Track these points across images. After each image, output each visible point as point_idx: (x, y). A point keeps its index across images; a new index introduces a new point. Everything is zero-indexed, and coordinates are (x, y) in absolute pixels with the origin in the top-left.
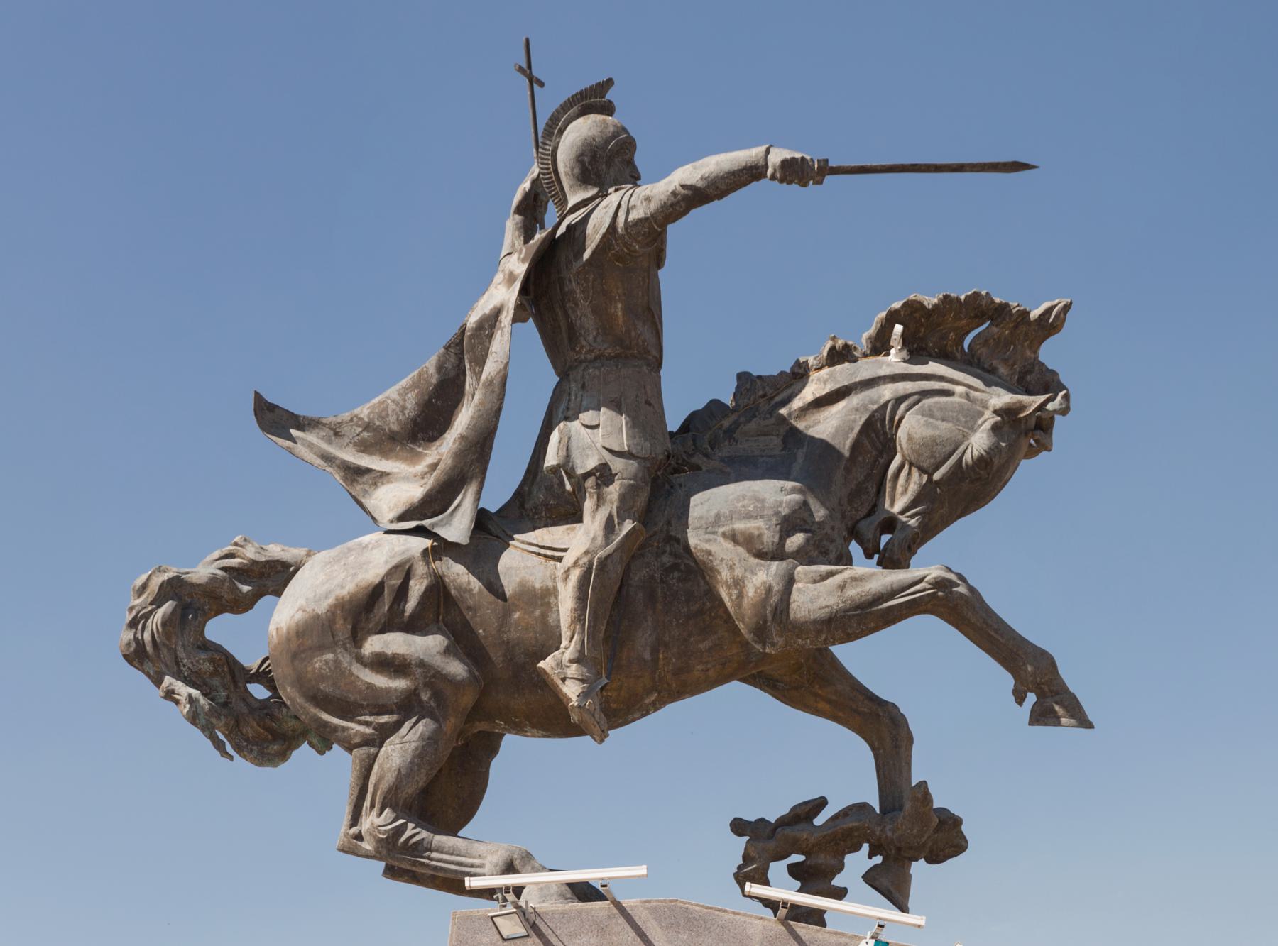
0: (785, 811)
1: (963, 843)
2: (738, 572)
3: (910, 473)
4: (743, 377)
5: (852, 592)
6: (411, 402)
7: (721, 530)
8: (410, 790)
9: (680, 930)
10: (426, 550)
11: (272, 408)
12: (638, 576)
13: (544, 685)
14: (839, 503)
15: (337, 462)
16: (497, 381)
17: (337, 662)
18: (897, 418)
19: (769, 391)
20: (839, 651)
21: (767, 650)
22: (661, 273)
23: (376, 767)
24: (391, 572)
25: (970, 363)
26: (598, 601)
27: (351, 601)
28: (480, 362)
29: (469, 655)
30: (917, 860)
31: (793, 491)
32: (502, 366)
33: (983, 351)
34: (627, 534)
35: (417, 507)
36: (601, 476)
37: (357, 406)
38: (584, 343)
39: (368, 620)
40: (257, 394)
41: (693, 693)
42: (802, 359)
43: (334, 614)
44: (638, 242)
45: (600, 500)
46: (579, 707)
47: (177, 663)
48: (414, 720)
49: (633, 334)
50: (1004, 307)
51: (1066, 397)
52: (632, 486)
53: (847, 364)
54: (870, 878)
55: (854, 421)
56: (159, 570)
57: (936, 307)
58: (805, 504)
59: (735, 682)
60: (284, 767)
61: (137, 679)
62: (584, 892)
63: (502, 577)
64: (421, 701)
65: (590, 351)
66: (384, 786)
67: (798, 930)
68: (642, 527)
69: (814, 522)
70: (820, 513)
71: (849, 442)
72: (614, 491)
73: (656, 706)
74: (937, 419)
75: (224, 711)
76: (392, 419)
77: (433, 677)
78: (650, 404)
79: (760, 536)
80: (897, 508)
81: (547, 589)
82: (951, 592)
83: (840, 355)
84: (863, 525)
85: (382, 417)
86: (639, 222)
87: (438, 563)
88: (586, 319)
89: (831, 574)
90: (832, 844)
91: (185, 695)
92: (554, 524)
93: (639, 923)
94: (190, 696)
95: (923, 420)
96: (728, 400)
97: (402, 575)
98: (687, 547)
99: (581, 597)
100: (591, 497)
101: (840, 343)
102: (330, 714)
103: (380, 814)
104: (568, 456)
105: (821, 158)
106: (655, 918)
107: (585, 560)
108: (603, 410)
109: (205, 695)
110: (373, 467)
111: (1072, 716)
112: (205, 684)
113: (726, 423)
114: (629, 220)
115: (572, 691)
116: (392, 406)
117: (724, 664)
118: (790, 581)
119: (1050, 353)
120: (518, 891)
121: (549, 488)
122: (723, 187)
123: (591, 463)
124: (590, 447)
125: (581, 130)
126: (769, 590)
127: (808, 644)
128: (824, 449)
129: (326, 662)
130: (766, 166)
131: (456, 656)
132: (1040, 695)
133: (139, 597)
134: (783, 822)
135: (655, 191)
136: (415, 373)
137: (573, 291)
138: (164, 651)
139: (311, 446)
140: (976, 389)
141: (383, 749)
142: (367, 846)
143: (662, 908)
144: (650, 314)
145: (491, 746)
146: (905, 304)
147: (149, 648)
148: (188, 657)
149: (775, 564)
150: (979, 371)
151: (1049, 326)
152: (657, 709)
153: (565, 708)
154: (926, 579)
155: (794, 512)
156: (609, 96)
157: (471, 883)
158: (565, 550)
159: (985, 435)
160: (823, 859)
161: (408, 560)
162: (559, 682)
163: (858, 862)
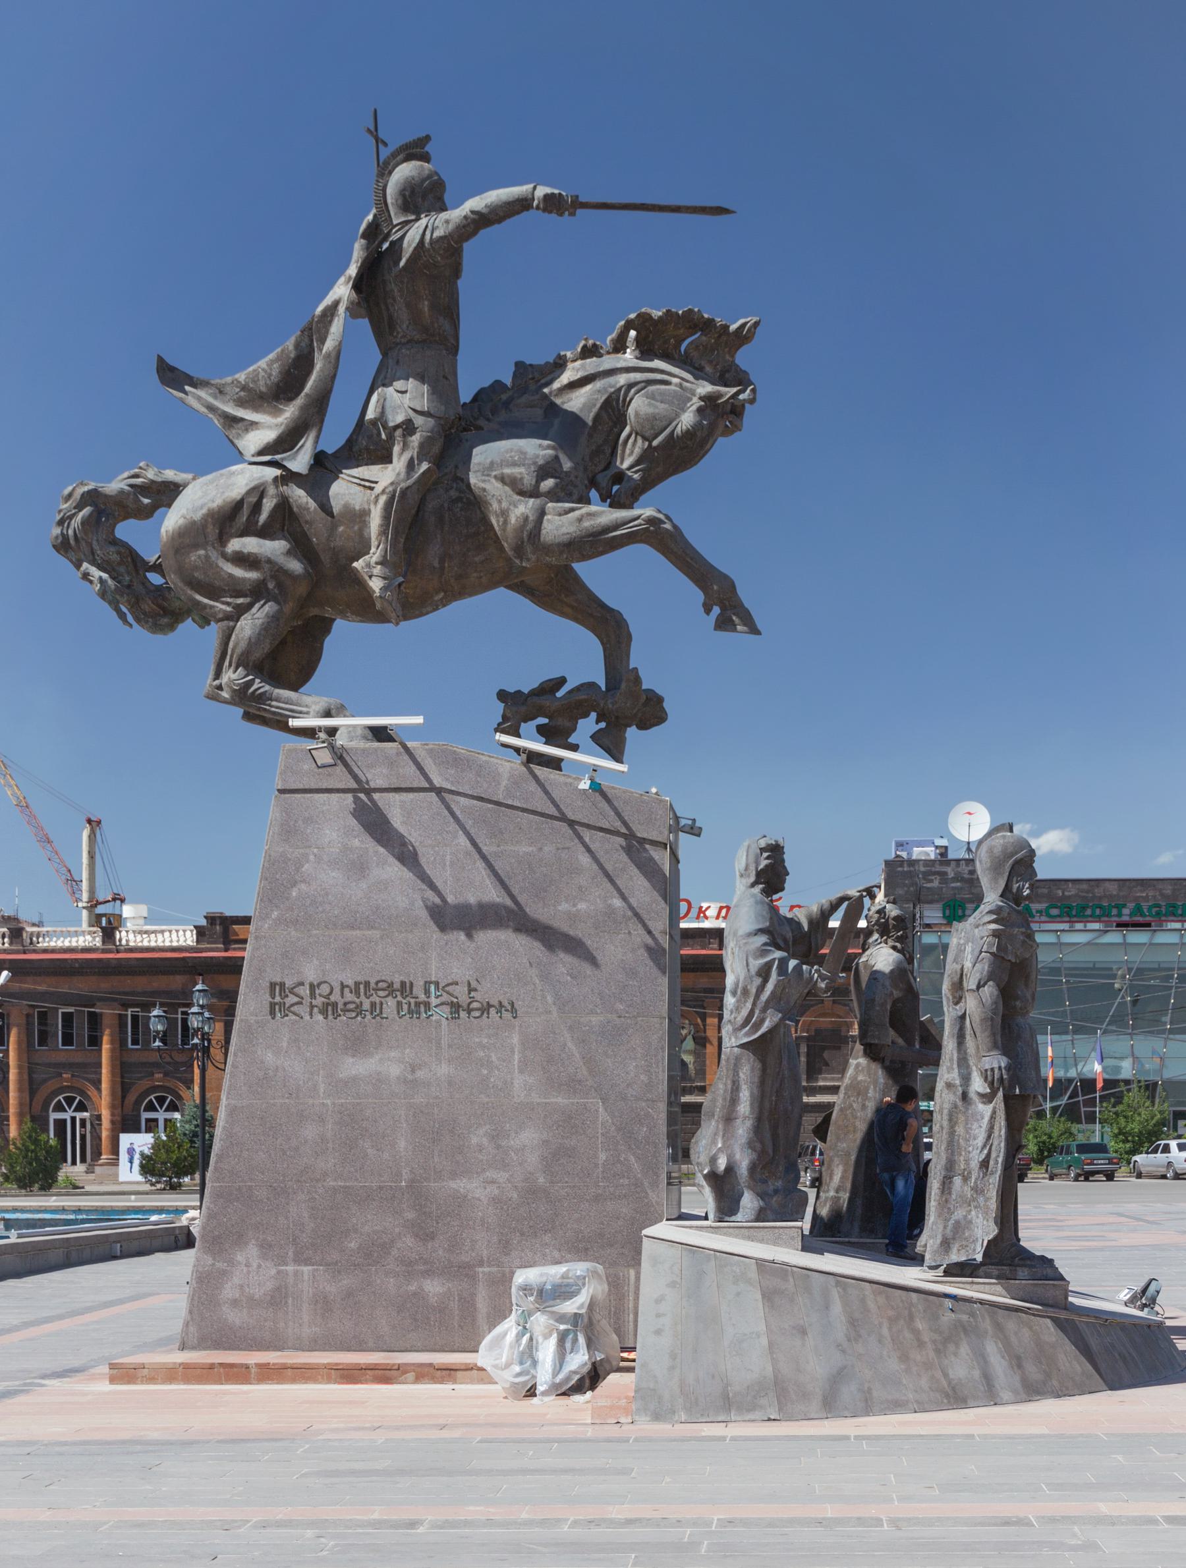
0: (536, 685)
2: (504, 505)
3: (635, 440)
4: (519, 365)
5: (587, 524)
6: (276, 370)
7: (494, 473)
8: (257, 654)
10: (276, 477)
11: (172, 369)
12: (431, 505)
13: (357, 582)
14: (583, 459)
15: (219, 412)
16: (333, 355)
17: (207, 557)
18: (628, 399)
19: (537, 375)
20: (581, 568)
21: (524, 564)
22: (459, 282)
23: (234, 636)
24: (250, 492)
25: (685, 363)
26: (399, 520)
27: (219, 512)
28: (323, 341)
29: (305, 557)
30: (630, 726)
31: (549, 447)
32: (337, 343)
33: (695, 354)
34: (424, 473)
36: (407, 428)
37: (238, 372)
38: (400, 330)
39: (231, 526)
40: (160, 360)
41: (471, 595)
42: (562, 353)
43: (206, 520)
44: (440, 255)
45: (405, 446)
46: (380, 597)
47: (93, 553)
48: (262, 602)
49: (436, 325)
50: (710, 322)
51: (753, 391)
52: (429, 437)
53: (594, 359)
54: (595, 737)
55: (597, 399)
56: (82, 484)
57: (660, 317)
58: (556, 458)
60: (172, 636)
61: (63, 563)
62: (380, 734)
63: (331, 500)
64: (267, 589)
65: (404, 337)
66: (239, 651)
67: (536, 771)
68: (435, 468)
69: (562, 471)
70: (567, 465)
71: (592, 415)
72: (415, 440)
73: (445, 603)
74: (657, 401)
75: (127, 591)
76: (262, 383)
77: (278, 572)
78: (447, 378)
79: (522, 479)
80: (625, 465)
81: (364, 510)
82: (660, 528)
83: (590, 352)
84: (600, 478)
85: (255, 381)
86: (441, 238)
87: (285, 487)
88: (401, 313)
89: (572, 510)
91: (97, 576)
92: (373, 464)
93: (419, 760)
94: (101, 578)
95: (647, 401)
96: (508, 381)
97: (258, 495)
98: (469, 485)
99: (386, 516)
100: (399, 444)
101: (591, 342)
102: (201, 595)
103: (235, 672)
104: (383, 412)
105: (573, 194)
107: (391, 489)
108: (411, 380)
109: (111, 577)
110: (246, 417)
111: (745, 625)
112: (114, 569)
113: (504, 397)
115: (376, 585)
116: (262, 374)
117: (493, 573)
118: (542, 513)
119: (744, 358)
120: (332, 731)
121: (370, 437)
122: (501, 214)
123: (400, 418)
124: (399, 407)
125: (404, 171)
126: (526, 519)
127: (553, 560)
128: (574, 419)
129: (199, 557)
130: (533, 199)
131: (296, 557)
132: (723, 609)
133: (66, 502)
134: (536, 693)
135: (453, 216)
136: (279, 350)
137: (392, 290)
138: (83, 543)
139: (199, 398)
140: (687, 381)
141: (239, 623)
142: (225, 694)
144: (451, 311)
145: (325, 626)
146: (639, 315)
147: (72, 542)
148: (101, 550)
149: (532, 501)
150: (691, 369)
151: (742, 337)
152: (444, 606)
153: (372, 597)
155: (548, 463)
157: (294, 723)
158: (376, 482)
159: (691, 415)
160: (562, 722)
161: (263, 484)
162: (367, 578)
163: (588, 725)
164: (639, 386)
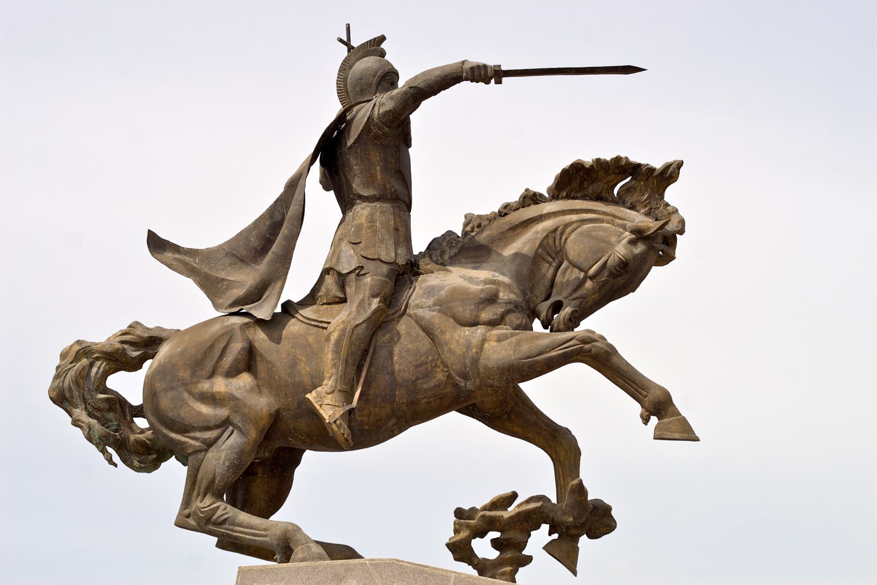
1: (614, 524)
9: (395, 581)
35: (242, 299)
54: (549, 548)
59: (454, 412)
90: (518, 523)
106: (378, 572)
114: (380, 112)
119: (672, 195)
143: (383, 565)
154: (577, 337)
156: (382, 46)
160: (512, 535)
163: (541, 536)
164: (575, 225)
